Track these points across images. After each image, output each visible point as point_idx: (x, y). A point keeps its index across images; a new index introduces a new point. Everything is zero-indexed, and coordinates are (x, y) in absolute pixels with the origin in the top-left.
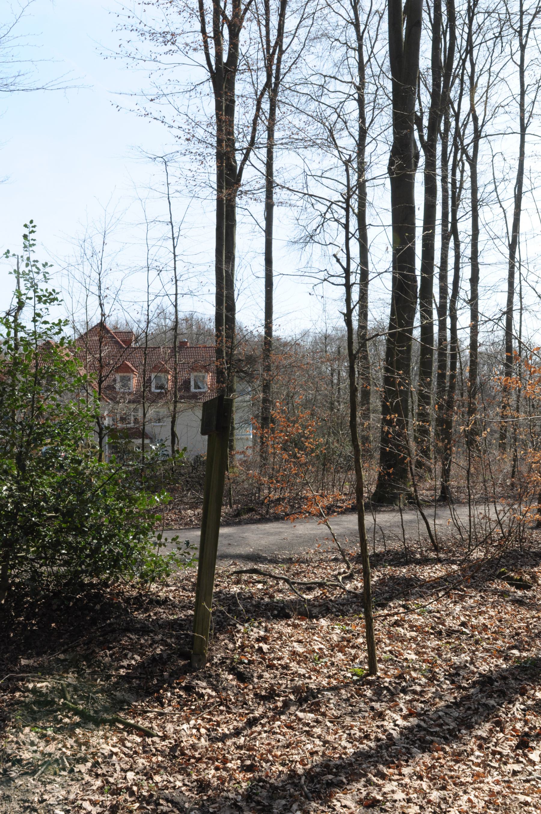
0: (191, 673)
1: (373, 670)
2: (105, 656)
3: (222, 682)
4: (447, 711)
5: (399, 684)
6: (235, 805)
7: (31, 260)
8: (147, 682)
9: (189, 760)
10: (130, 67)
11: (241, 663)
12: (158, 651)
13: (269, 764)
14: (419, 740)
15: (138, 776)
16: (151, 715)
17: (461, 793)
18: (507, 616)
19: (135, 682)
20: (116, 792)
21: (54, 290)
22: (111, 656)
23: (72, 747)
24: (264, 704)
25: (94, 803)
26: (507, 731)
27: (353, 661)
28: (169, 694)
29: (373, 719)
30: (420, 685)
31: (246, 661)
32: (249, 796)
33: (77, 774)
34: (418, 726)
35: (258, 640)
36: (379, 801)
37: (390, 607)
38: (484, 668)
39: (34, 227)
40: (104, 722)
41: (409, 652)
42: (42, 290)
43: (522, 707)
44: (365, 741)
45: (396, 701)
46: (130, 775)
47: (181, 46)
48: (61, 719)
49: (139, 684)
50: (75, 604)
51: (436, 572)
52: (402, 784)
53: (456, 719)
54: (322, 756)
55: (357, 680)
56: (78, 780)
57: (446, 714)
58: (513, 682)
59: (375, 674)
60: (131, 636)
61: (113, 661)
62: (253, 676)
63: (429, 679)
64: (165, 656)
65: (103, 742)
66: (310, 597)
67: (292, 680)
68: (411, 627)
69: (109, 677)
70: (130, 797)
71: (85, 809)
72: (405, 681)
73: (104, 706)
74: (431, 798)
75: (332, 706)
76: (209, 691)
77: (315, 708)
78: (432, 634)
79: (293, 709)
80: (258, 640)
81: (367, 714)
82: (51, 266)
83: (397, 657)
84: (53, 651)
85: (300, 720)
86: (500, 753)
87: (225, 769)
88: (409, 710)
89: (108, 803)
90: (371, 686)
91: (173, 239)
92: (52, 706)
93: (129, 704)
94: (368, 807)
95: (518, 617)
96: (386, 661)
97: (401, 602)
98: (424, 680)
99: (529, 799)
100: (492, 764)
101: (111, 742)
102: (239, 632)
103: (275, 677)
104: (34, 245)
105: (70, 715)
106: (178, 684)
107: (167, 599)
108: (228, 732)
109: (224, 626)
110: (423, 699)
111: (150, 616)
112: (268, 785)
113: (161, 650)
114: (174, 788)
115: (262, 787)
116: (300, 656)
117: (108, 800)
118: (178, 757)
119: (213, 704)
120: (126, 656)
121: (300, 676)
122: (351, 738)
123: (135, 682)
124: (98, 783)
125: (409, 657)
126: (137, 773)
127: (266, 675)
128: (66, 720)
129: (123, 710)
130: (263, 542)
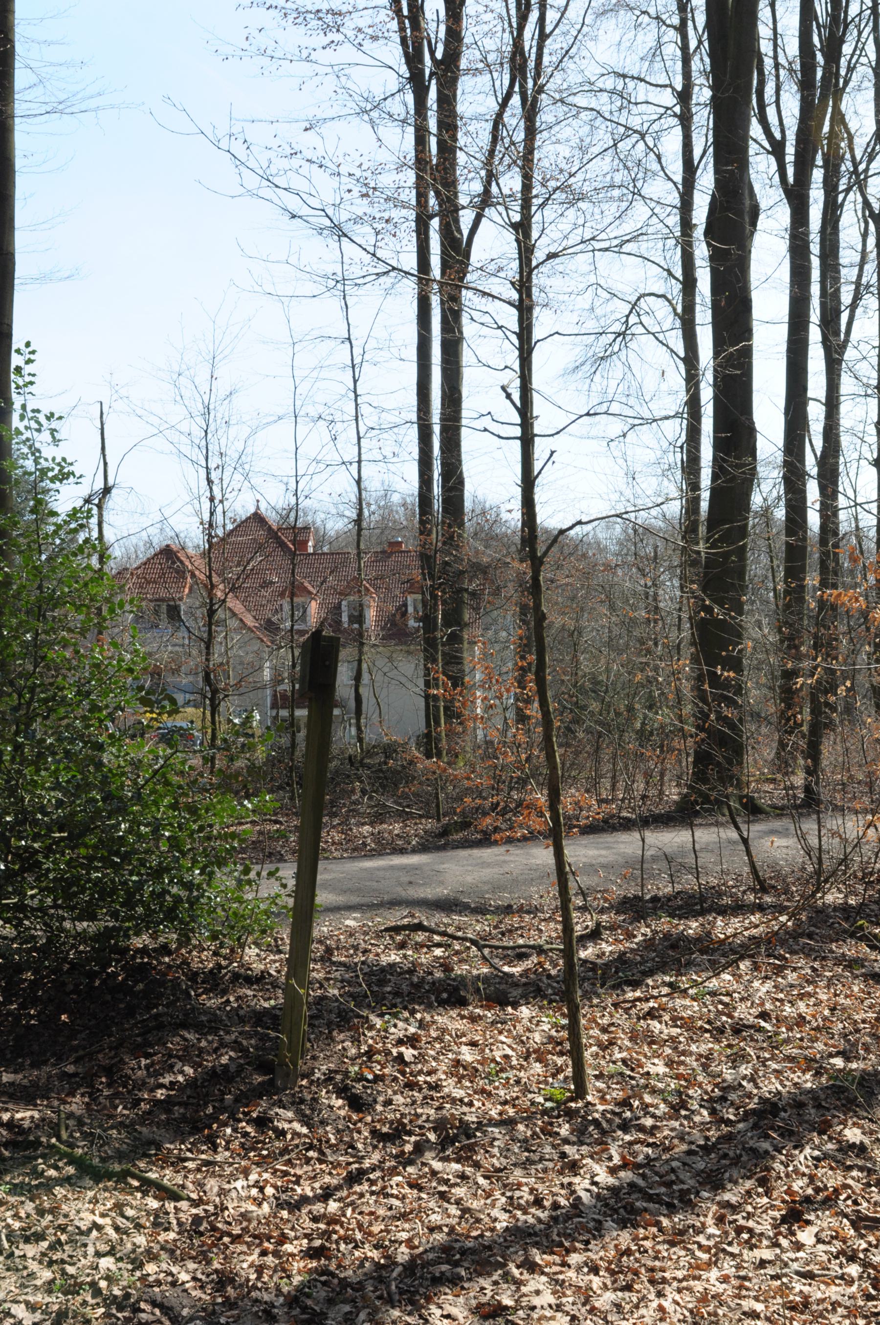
0: (270, 1095)
1: (580, 1092)
2: (137, 1067)
3: (320, 1111)
4: (688, 1160)
5: (619, 1115)
6: (269, 1314)
7: (29, 409)
8: (197, 1111)
9: (221, 1239)
10: (266, 73)
11: (360, 1078)
12: (224, 1060)
13: (350, 1246)
14: (624, 1207)
15: (120, 1265)
16: (191, 1165)
17: (652, 1296)
18: (848, 1002)
19: (178, 1111)
20: (72, 1288)
21: (64, 459)
22: (147, 1067)
23: (28, 1216)
24: (384, 1147)
25: (32, 1307)
26: (775, 1194)
27: (554, 1076)
28: (229, 1131)
29: (561, 1173)
30: (653, 1116)
31: (370, 1077)
32: (294, 1300)
33: (17, 1260)
34: (632, 1185)
35: (400, 1042)
36: (506, 1308)
37: (647, 986)
38: (770, 1086)
39: (33, 352)
40: (109, 1176)
41: (656, 1061)
42: (46, 460)
43: (816, 1153)
44: (533, 1210)
45: (606, 1144)
46: (106, 1263)
47: (351, 34)
48: (43, 1171)
49: (184, 1115)
50: (104, 982)
51: (753, 925)
52: (557, 1281)
53: (699, 1173)
54: (448, 1234)
55: (552, 1109)
56: (17, 1270)
57: (684, 1164)
58: (813, 1111)
59: (583, 1098)
60: (187, 1036)
61: (149, 1075)
62: (375, 1101)
63: (672, 1107)
64: (233, 1068)
65: (85, 1208)
66: (516, 970)
67: (439, 1108)
68: (674, 1019)
69: (137, 1103)
70: (93, 1297)
71: (14, 1317)
72: (631, 1110)
73: (118, 1151)
74: (597, 1305)
75: (495, 1151)
76: (297, 1126)
77: (465, 1156)
78: (707, 1031)
79: (429, 1155)
80: (400, 1042)
81: (550, 1165)
82: (60, 418)
83: (632, 1070)
84: (60, 1059)
85: (434, 1173)
86: (750, 1231)
87: (276, 1254)
88: (623, 1158)
89: (56, 1307)
90: (573, 1118)
91: (353, 367)
92: (36, 1149)
93: (159, 1147)
94: (485, 1317)
95: (867, 1003)
96: (611, 1077)
97: (667, 979)
98: (663, 1108)
99: (759, 1307)
100: (729, 1249)
101: (100, 1208)
102: (371, 1027)
103: (414, 1103)
104: (32, 383)
105: (60, 1164)
106: (245, 1114)
107: (264, 974)
108: (311, 1194)
109: (343, 1018)
110: (651, 1141)
111: (228, 1002)
112: (336, 1281)
113: (231, 1058)
114: (174, 1284)
115: (324, 1283)
116: (465, 1068)
117: (55, 1301)
118: (205, 1235)
119: (297, 1146)
120: (172, 1066)
121: (453, 1101)
122: (511, 1204)
123: (178, 1111)
124: (47, 1275)
125: (653, 1070)
126: (120, 1259)
127: (399, 1099)
128: (52, 1173)
129: (145, 1155)
130: (469, 879)
